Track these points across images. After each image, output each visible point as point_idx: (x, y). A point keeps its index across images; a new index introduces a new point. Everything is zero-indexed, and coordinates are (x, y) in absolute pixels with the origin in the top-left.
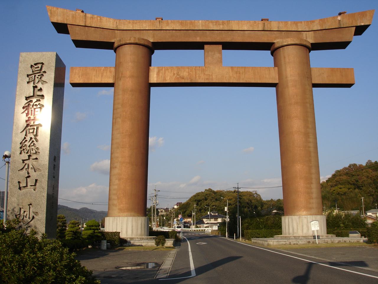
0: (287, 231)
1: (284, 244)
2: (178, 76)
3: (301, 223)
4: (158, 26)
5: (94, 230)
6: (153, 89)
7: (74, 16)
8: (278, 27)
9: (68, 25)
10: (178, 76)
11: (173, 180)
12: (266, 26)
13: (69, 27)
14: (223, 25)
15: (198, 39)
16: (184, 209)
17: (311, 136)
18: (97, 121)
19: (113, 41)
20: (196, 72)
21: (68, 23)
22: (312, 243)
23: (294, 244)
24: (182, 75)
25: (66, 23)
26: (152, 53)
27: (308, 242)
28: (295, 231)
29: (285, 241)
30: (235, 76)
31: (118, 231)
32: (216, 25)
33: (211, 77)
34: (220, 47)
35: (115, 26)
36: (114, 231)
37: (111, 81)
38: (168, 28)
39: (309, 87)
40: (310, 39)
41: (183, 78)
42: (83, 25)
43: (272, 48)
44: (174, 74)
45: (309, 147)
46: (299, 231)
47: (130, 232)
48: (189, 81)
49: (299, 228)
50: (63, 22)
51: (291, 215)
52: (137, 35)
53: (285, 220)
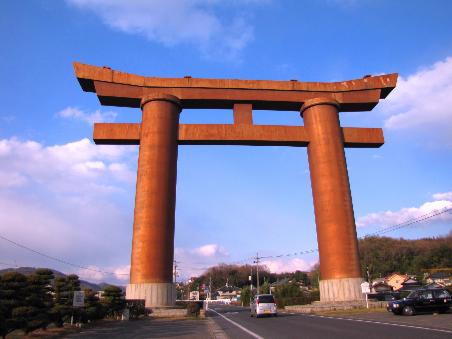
0: (327, 296)
1: (329, 311)
2: (207, 134)
3: (342, 287)
4: (187, 84)
5: (115, 296)
6: (180, 148)
7: (101, 72)
8: (307, 88)
9: (94, 82)
10: (207, 134)
11: (194, 258)
12: (295, 86)
13: (96, 84)
14: (252, 84)
15: (228, 98)
16: (198, 283)
17: (347, 194)
18: (117, 172)
19: (140, 97)
20: (226, 131)
21: (95, 79)
22: (358, 308)
23: (340, 310)
24: (211, 132)
25: (92, 78)
26: (181, 111)
27: (78, 301)
28: (336, 295)
29: (329, 307)
30: (266, 134)
31: (142, 298)
32: (246, 84)
33: (241, 135)
34: (250, 106)
35: (143, 83)
36: (137, 298)
37: (137, 138)
38: (196, 86)
39: (340, 145)
40: (339, 99)
41: (212, 136)
42: (110, 81)
43: (302, 109)
44: (203, 131)
45: (346, 206)
46: (340, 295)
47: (154, 300)
48: (218, 139)
49: (340, 292)
50: (89, 78)
51: (331, 278)
52: (166, 91)
53: (324, 284)
